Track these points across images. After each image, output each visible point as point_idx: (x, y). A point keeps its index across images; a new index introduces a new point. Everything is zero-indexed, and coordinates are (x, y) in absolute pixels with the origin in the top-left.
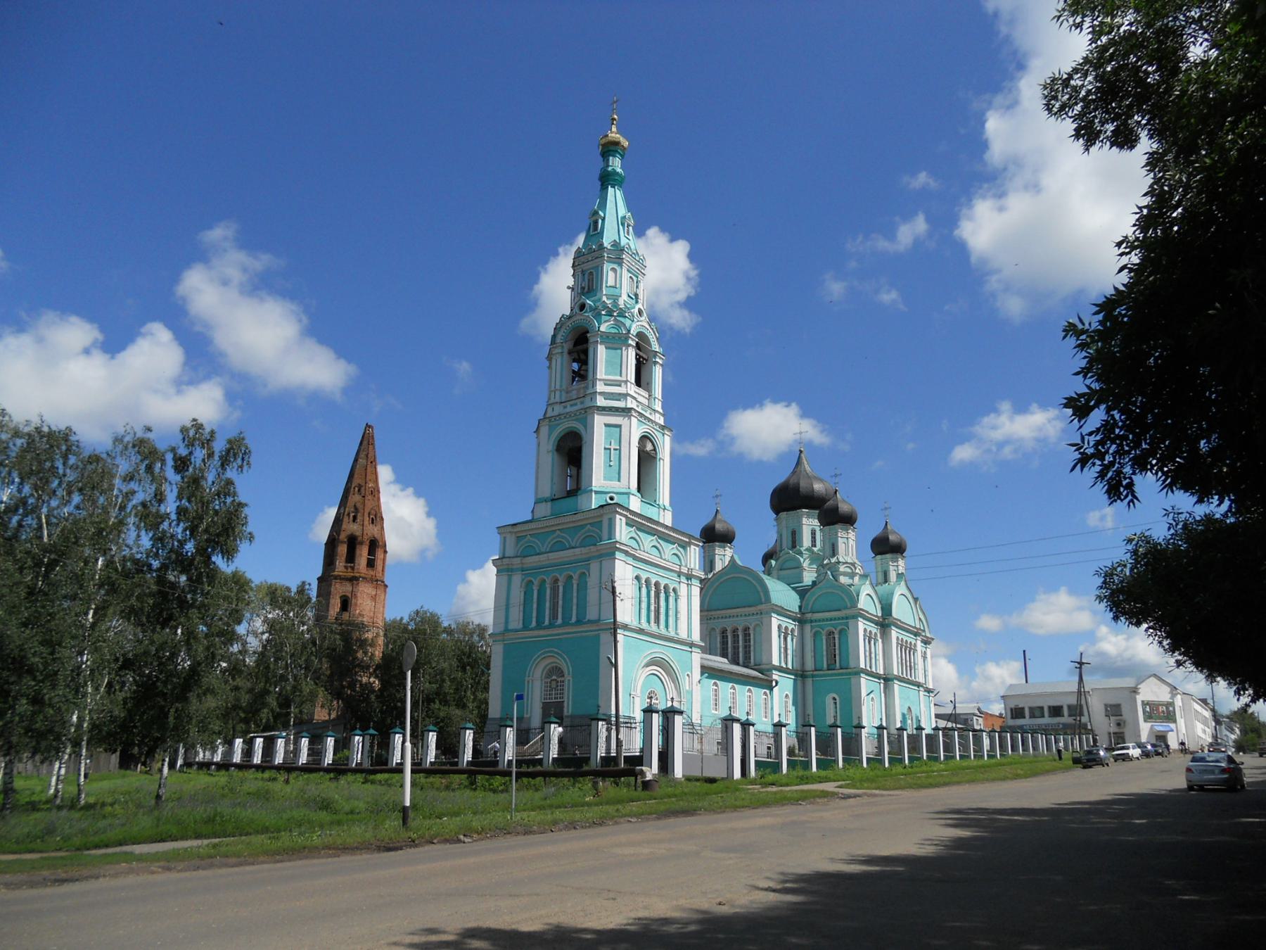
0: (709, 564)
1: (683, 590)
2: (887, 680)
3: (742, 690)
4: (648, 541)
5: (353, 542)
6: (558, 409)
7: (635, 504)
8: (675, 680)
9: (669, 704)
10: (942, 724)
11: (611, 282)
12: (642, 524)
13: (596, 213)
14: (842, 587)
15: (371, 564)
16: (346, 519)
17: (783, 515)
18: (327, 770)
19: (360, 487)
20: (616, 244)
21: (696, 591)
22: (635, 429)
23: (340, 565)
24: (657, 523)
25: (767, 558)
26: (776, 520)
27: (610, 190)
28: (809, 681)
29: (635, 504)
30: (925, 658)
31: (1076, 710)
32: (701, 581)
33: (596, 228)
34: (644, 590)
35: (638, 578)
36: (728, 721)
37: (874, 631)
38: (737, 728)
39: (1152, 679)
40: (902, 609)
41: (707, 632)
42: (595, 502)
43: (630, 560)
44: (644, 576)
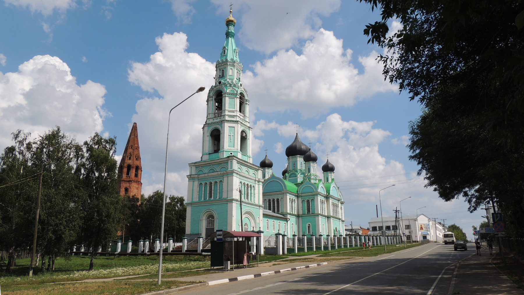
0: (264, 176)
1: (256, 186)
2: (328, 217)
3: (277, 222)
4: (244, 169)
5: (129, 167)
6: (211, 121)
7: (240, 156)
8: (254, 219)
9: (252, 230)
10: (348, 233)
11: (230, 74)
12: (242, 163)
13: (224, 47)
14: (312, 184)
15: (136, 175)
16: (127, 158)
17: (290, 157)
18: (130, 254)
19: (132, 146)
20: (232, 59)
21: (261, 187)
22: (239, 129)
23: (124, 176)
24: (247, 162)
25: (284, 173)
26: (288, 159)
27: (230, 38)
28: (300, 219)
29: (240, 156)
30: (341, 209)
31: (395, 228)
32: (263, 182)
33: (224, 53)
34: (243, 187)
35: (241, 182)
36: (277, 235)
37: (324, 200)
38: (281, 236)
39: (422, 216)
40: (333, 192)
41: (264, 201)
42: (225, 155)
43: (238, 176)
44: (243, 182)
